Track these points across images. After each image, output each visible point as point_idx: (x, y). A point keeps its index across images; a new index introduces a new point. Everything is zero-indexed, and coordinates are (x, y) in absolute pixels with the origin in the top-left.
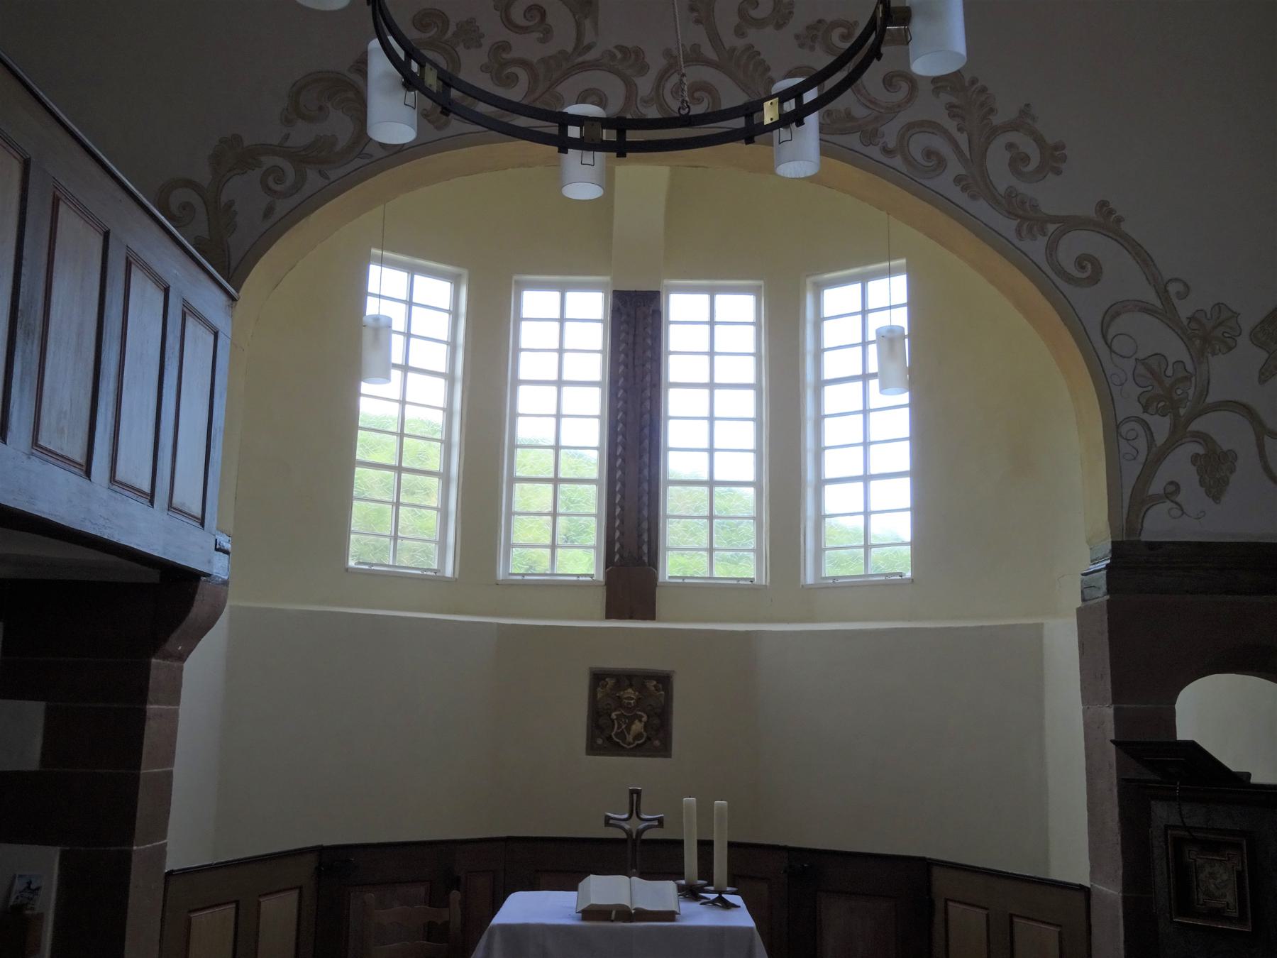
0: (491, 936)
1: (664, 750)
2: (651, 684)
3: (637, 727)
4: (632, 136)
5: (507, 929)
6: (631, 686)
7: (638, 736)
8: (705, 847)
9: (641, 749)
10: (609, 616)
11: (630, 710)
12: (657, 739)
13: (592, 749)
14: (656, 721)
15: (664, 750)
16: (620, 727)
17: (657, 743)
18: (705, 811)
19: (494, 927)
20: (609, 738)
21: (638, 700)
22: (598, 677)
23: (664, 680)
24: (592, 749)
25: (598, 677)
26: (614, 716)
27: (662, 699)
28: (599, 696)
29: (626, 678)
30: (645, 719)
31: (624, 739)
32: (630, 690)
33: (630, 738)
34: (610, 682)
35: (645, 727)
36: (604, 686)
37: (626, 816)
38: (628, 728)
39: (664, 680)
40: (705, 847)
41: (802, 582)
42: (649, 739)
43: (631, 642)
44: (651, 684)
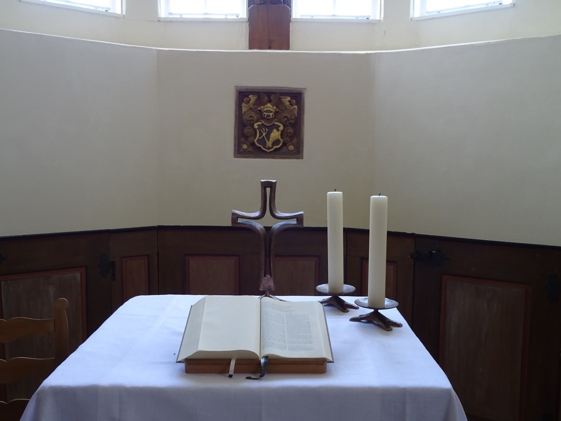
0: (39, 403)
1: (298, 153)
2: (287, 100)
3: (275, 134)
4: (268, 259)
5: (66, 394)
6: (270, 101)
7: (276, 142)
8: (356, 239)
9: (280, 151)
10: (250, 48)
11: (269, 121)
12: (291, 144)
13: (239, 152)
14: (291, 130)
15: (298, 153)
16: (261, 134)
17: (291, 148)
18: (356, 202)
19: (43, 391)
20: (253, 144)
21: (276, 113)
22: (242, 95)
23: (297, 96)
24: (239, 152)
25: (242, 95)
26: (256, 126)
27: (296, 112)
28: (244, 109)
29: (265, 95)
30: (281, 128)
31: (264, 144)
32: (269, 105)
33: (269, 144)
34: (253, 98)
35: (282, 135)
36: (248, 102)
37: (257, 214)
38: (268, 136)
39: (297, 96)
40: (356, 239)
41: (411, 15)
42: (284, 144)
43: (269, 70)
44: (287, 100)
